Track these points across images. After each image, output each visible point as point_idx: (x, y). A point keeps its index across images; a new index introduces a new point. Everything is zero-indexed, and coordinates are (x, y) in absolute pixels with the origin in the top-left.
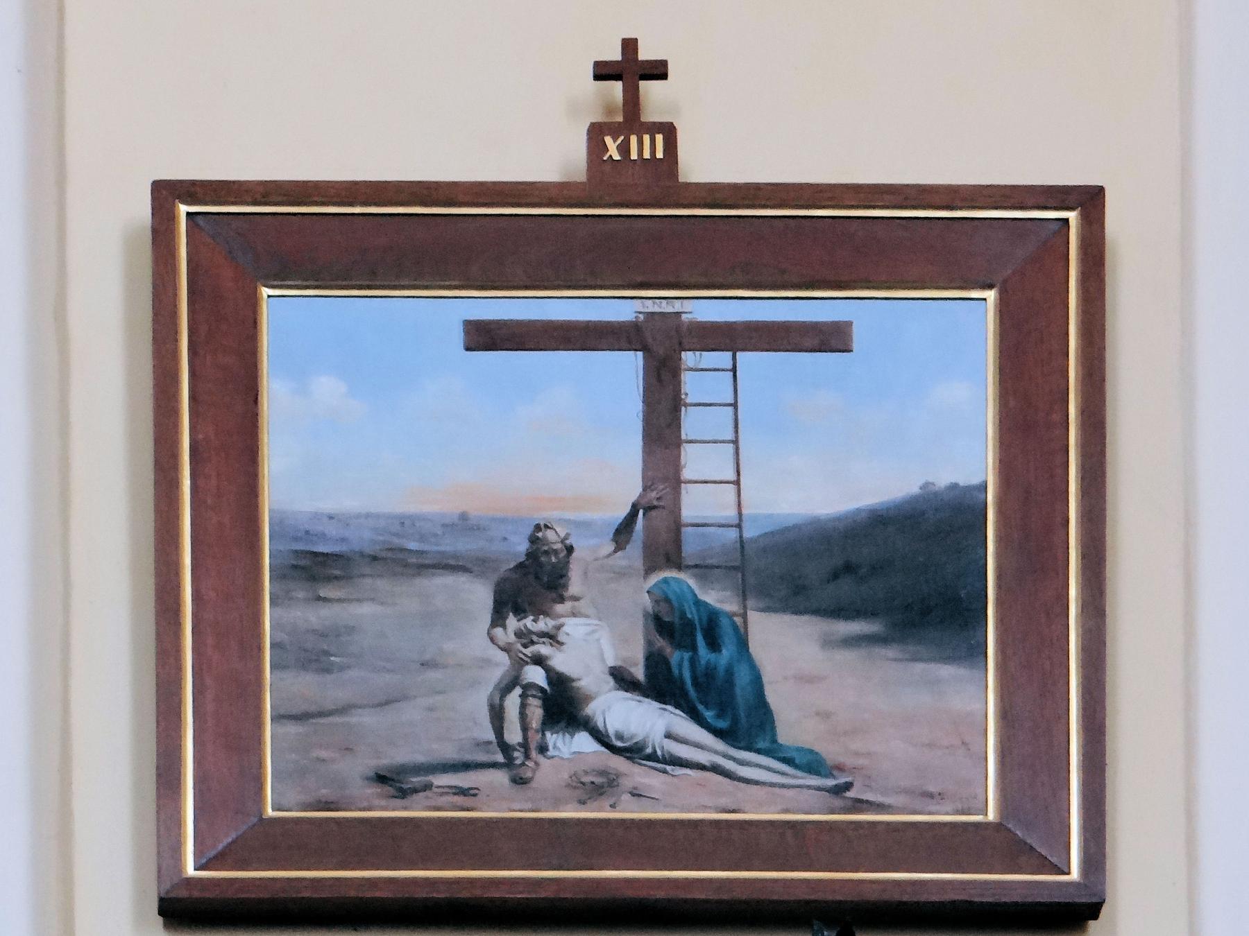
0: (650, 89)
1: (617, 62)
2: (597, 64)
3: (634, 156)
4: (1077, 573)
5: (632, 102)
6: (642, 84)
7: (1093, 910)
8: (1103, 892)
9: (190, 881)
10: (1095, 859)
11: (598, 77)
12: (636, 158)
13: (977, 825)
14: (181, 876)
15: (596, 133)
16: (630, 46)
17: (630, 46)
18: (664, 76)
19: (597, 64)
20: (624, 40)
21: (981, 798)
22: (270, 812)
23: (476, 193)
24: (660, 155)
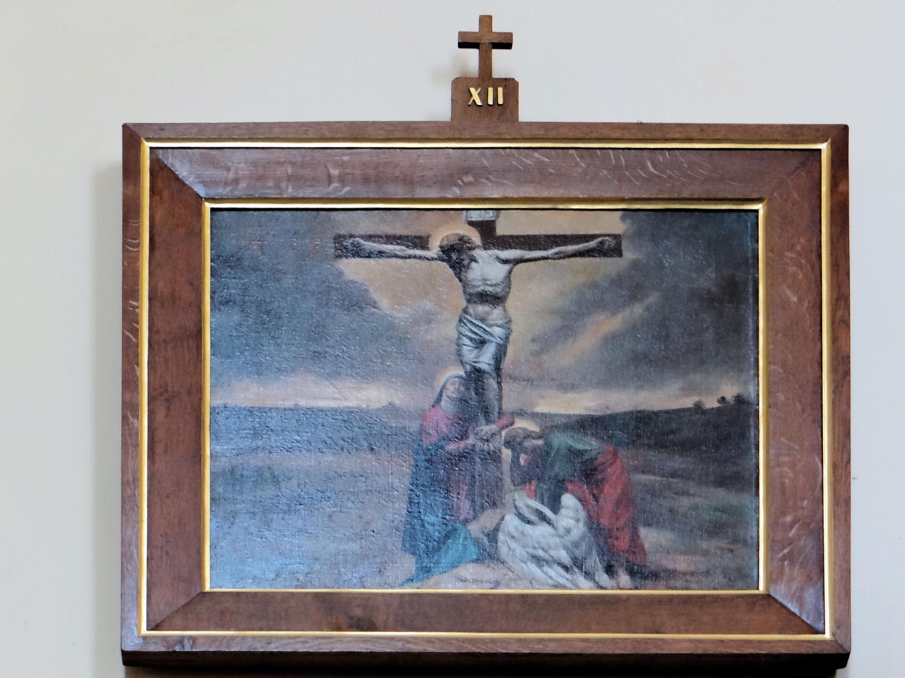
0: (498, 55)
1: (476, 33)
2: (461, 34)
3: (490, 102)
4: (828, 468)
5: (486, 63)
6: (495, 52)
7: (841, 659)
8: (850, 648)
9: (145, 638)
10: (843, 623)
11: (462, 45)
12: (491, 103)
13: (755, 595)
14: (476, 78)
15: (461, 86)
16: (486, 21)
17: (486, 21)
18: (508, 46)
19: (461, 34)
20: (490, 17)
21: (755, 535)
22: (208, 588)
23: (255, 271)
24: (501, 101)
